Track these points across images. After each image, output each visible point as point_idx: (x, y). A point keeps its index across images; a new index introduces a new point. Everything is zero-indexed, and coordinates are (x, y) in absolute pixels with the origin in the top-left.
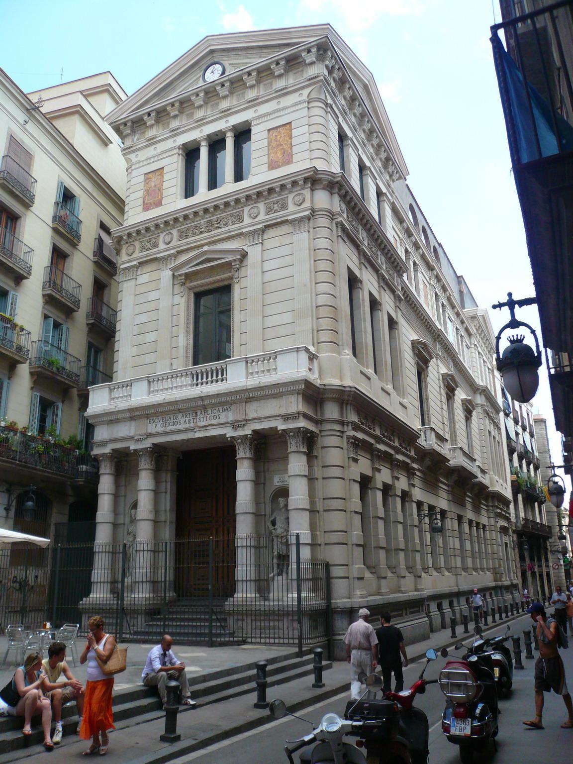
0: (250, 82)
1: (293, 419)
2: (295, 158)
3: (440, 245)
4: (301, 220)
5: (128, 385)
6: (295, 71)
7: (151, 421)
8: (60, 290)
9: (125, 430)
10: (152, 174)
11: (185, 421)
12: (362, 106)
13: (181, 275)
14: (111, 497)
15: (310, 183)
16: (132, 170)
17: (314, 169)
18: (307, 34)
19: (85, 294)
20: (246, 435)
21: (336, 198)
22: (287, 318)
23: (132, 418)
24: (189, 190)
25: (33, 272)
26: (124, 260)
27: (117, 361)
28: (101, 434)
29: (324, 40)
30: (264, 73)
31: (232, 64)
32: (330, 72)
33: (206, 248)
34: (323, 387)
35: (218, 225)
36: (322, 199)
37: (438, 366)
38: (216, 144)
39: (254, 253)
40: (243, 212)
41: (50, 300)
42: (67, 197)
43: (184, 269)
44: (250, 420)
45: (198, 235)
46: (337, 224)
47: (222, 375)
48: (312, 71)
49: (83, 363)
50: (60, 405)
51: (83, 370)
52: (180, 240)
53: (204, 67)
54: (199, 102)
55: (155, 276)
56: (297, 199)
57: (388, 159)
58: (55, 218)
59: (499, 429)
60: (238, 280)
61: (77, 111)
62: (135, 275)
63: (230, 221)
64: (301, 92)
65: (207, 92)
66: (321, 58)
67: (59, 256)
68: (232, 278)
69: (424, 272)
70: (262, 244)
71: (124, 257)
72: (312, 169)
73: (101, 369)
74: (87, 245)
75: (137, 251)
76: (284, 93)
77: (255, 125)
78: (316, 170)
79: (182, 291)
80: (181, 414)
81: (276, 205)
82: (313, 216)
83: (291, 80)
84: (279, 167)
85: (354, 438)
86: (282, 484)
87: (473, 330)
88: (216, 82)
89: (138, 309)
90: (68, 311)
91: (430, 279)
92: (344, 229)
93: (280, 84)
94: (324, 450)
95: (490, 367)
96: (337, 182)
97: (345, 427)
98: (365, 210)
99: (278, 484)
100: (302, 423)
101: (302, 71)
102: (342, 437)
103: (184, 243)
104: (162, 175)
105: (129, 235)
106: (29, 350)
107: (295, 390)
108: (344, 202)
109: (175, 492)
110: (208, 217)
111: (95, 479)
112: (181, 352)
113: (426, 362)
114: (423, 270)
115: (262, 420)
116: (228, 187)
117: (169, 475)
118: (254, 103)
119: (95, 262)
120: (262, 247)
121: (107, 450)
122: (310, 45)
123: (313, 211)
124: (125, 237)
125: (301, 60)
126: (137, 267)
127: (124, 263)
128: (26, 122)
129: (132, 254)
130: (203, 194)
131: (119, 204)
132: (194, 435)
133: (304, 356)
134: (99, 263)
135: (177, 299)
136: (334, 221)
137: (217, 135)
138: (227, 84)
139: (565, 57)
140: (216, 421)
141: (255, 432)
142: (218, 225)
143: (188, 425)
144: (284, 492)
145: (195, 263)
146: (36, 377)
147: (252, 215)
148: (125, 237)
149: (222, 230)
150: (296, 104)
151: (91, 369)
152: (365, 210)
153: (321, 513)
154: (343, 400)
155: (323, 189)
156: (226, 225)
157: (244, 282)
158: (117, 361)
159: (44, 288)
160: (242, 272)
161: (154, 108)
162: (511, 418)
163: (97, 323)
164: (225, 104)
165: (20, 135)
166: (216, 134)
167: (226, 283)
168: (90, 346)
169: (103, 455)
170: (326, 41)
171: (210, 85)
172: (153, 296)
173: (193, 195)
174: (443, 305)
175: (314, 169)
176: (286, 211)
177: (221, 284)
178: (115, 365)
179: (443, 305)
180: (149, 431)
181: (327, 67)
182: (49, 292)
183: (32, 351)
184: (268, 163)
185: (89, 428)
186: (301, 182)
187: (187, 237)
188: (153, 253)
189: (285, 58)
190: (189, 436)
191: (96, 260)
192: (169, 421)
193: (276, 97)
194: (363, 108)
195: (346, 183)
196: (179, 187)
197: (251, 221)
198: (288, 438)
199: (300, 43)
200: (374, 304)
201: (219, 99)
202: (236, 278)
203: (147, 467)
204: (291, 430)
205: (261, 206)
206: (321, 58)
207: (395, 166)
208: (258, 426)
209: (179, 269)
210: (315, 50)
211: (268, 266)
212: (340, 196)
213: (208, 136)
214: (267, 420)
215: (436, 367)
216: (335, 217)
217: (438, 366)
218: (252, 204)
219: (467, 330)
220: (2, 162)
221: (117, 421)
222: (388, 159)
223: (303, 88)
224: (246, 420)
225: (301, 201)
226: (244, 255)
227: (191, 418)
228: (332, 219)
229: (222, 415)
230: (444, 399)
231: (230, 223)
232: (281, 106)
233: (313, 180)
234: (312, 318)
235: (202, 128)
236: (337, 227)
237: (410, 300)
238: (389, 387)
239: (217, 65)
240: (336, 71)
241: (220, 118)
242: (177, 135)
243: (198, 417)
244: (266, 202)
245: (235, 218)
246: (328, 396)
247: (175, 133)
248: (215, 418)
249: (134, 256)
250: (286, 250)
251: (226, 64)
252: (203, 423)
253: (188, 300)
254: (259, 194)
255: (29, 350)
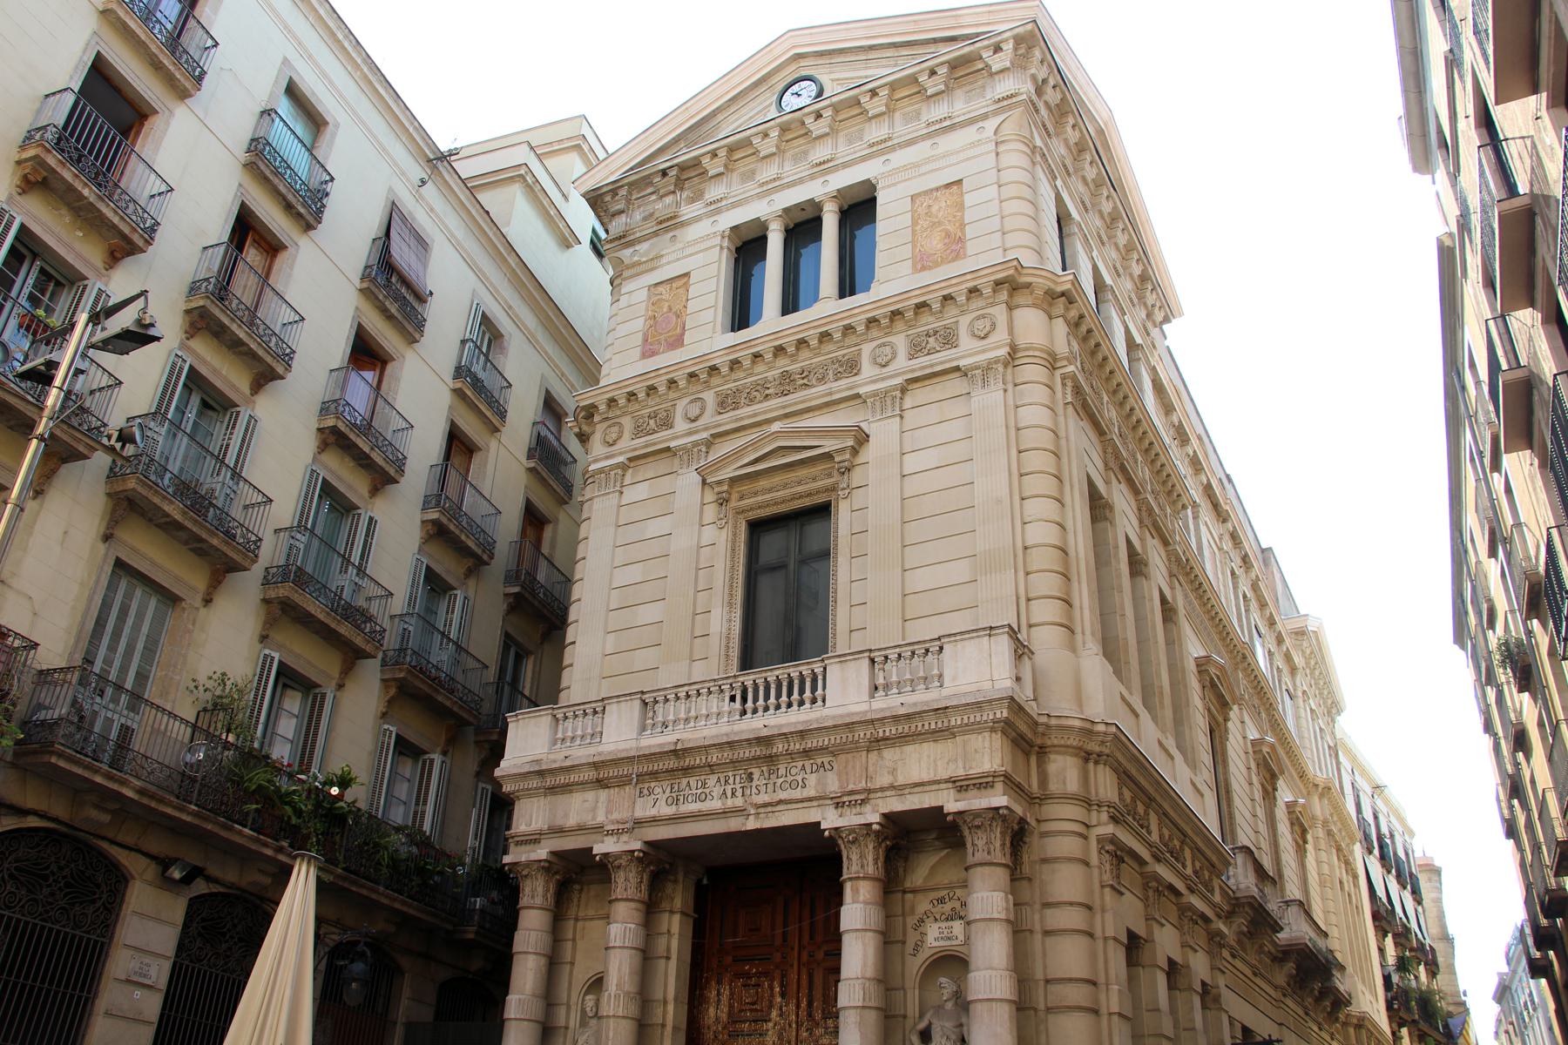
0: (874, 108)
1: (979, 788)
2: (971, 248)
3: (1228, 477)
4: (988, 368)
5: (598, 709)
6: (968, 88)
7: (645, 792)
8: (456, 511)
9: (582, 808)
10: (664, 285)
11: (724, 793)
12: (1097, 164)
13: (719, 483)
14: (543, 961)
15: (1005, 292)
16: (625, 279)
17: (1015, 263)
18: (992, 18)
19: (507, 528)
20: (869, 825)
21: (1060, 327)
22: (961, 571)
23: (601, 784)
24: (742, 314)
25: (407, 469)
26: (597, 456)
27: (571, 665)
28: (530, 816)
29: (1029, 27)
30: (908, 89)
31: (838, 80)
32: (1039, 91)
33: (776, 427)
34: (1043, 720)
35: (805, 381)
36: (1032, 326)
37: (1242, 722)
38: (803, 228)
39: (883, 433)
40: (859, 355)
41: (438, 534)
42: (488, 333)
43: (729, 470)
44: (875, 791)
45: (760, 402)
46: (1064, 377)
47: (814, 689)
48: (1005, 86)
49: (491, 674)
50: (437, 758)
51: (491, 690)
52: (720, 413)
53: (780, 87)
54: (767, 147)
55: (664, 485)
56: (980, 324)
57: (1144, 278)
58: (460, 372)
59: (1355, 877)
60: (847, 491)
61: (518, 176)
62: (618, 484)
63: (831, 373)
64: (981, 124)
65: (784, 129)
66: (1020, 62)
67: (458, 445)
68: (833, 489)
69: (1209, 523)
70: (902, 417)
71: (597, 447)
72: (1010, 264)
73: (527, 692)
74: (523, 412)
75: (627, 435)
76: (949, 127)
77: (883, 188)
78: (1019, 267)
79: (722, 516)
80: (715, 777)
81: (931, 340)
82: (1013, 359)
83: (960, 105)
84: (937, 265)
85: (1113, 840)
86: (948, 943)
87: (1298, 660)
88: (806, 110)
89: (621, 556)
90: (475, 560)
91: (1220, 539)
92: (1078, 390)
93: (938, 111)
94: (1045, 867)
95: (1332, 745)
96: (1063, 294)
97: (1094, 814)
98: (1115, 360)
99: (937, 944)
100: (998, 798)
101: (983, 87)
102: (1086, 838)
103: (728, 420)
104: (686, 286)
105: (612, 402)
106: (385, 630)
107: (986, 722)
108: (1076, 337)
109: (689, 960)
110: (783, 364)
111: (509, 923)
112: (715, 645)
113: (1224, 705)
114: (1207, 519)
115: (907, 791)
116: (826, 306)
117: (677, 918)
118: (882, 148)
119: (531, 470)
120: (901, 424)
121: (541, 853)
122: (999, 38)
123: (1014, 349)
124: (602, 407)
125: (980, 66)
126: (624, 467)
127: (596, 461)
128: (423, 182)
129: (615, 441)
130: (770, 320)
131: (586, 364)
132: (744, 824)
133: (1003, 644)
134: (538, 473)
135: (709, 534)
136: (1058, 373)
137: (803, 209)
138: (827, 113)
139: (1460, 140)
140: (797, 794)
141: (889, 817)
142: (805, 381)
143: (730, 803)
144: (954, 963)
145: (752, 457)
146: (393, 691)
147: (879, 360)
148: (602, 407)
149: (813, 390)
150: (973, 145)
151: (507, 688)
152: (1115, 360)
153: (1041, 1014)
154: (1089, 753)
155: (1034, 305)
156: (822, 380)
157: (858, 498)
158: (571, 665)
159: (425, 507)
160: (857, 477)
161: (676, 161)
162: (1375, 857)
163: (527, 595)
164: (821, 152)
165: (408, 203)
166: (800, 207)
167: (820, 499)
168: (508, 641)
169: (529, 864)
170: (1031, 31)
171: (791, 115)
172: (654, 528)
173: (747, 326)
174: (1245, 596)
175: (1015, 263)
176: (954, 350)
177: (807, 502)
178: (565, 673)
179: (1245, 596)
180: (639, 814)
181: (1034, 77)
182: (435, 516)
183: (391, 631)
184: (913, 257)
185: (502, 806)
186: (987, 291)
187: (736, 406)
188: (661, 438)
189: (947, 62)
190: (734, 825)
191: (533, 465)
192: (687, 792)
193: (929, 136)
194: (1099, 169)
195: (1080, 296)
196: (720, 311)
197: (877, 371)
198: (966, 833)
199: (978, 35)
200: (1137, 565)
201: (809, 142)
202: (843, 489)
203: (631, 893)
204: (977, 814)
205: (900, 341)
206: (1020, 62)
207: (1158, 294)
208: (896, 805)
209: (717, 470)
210: (1011, 46)
211: (912, 463)
212: (1068, 323)
213: (786, 210)
214: (917, 789)
215: (1239, 724)
216: (1058, 365)
217: (1242, 722)
218: (879, 338)
219: (1288, 657)
220: (371, 248)
221: (567, 788)
222: (1144, 278)
223: (985, 117)
224: (869, 791)
225: (988, 329)
226: (862, 438)
227: (738, 786)
228: (1054, 369)
229: (812, 779)
230: (1258, 795)
231: (831, 375)
232: (940, 150)
233: (1011, 286)
234: (1016, 571)
235: (773, 197)
236: (1064, 385)
237: (1191, 572)
238: (1170, 743)
239: (808, 83)
240: (1049, 90)
241: (812, 177)
242: (718, 211)
243: (754, 784)
244: (909, 333)
245: (841, 366)
246: (1056, 742)
247: (716, 208)
248: (793, 785)
249: (621, 445)
250: (955, 430)
251: (825, 79)
252: (763, 798)
253: (735, 534)
254: (896, 314)
255: (385, 630)
